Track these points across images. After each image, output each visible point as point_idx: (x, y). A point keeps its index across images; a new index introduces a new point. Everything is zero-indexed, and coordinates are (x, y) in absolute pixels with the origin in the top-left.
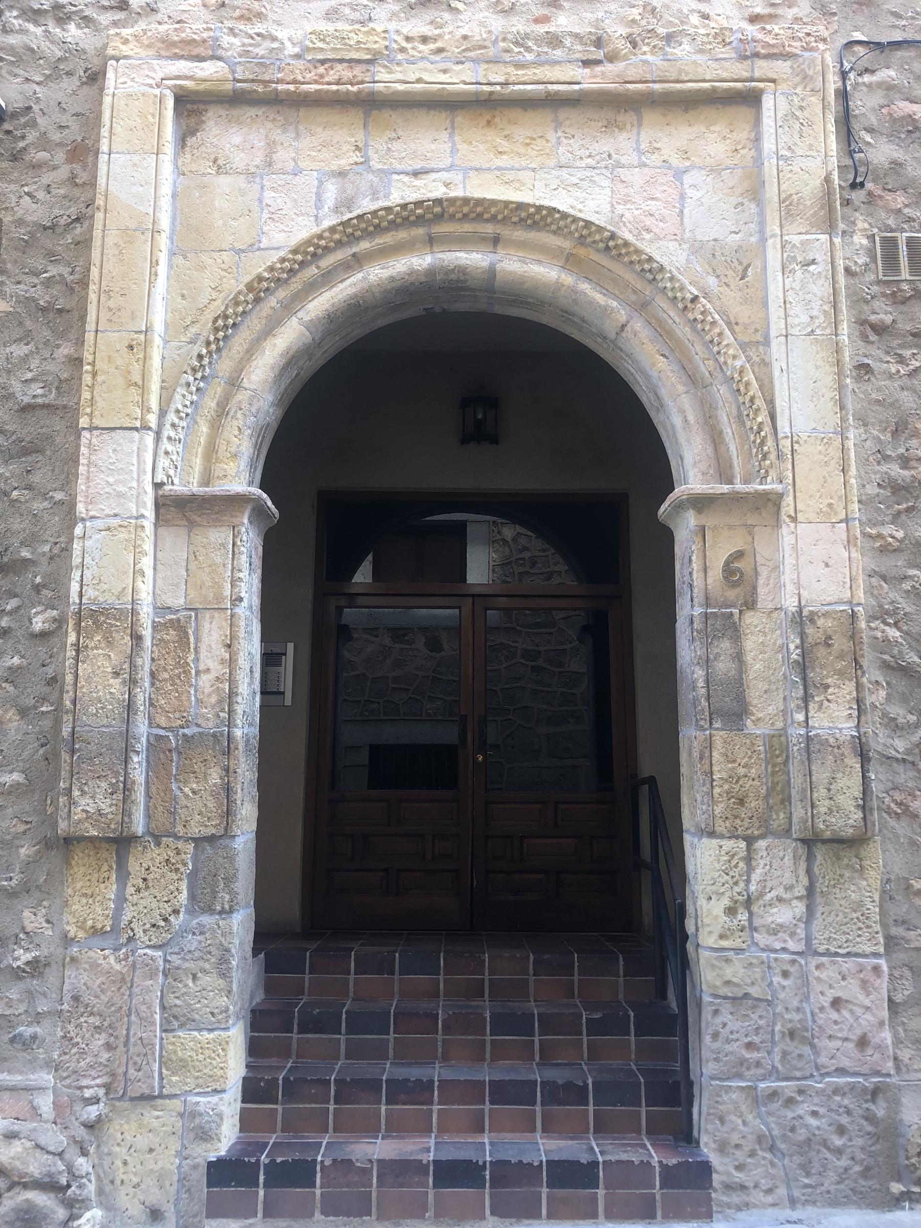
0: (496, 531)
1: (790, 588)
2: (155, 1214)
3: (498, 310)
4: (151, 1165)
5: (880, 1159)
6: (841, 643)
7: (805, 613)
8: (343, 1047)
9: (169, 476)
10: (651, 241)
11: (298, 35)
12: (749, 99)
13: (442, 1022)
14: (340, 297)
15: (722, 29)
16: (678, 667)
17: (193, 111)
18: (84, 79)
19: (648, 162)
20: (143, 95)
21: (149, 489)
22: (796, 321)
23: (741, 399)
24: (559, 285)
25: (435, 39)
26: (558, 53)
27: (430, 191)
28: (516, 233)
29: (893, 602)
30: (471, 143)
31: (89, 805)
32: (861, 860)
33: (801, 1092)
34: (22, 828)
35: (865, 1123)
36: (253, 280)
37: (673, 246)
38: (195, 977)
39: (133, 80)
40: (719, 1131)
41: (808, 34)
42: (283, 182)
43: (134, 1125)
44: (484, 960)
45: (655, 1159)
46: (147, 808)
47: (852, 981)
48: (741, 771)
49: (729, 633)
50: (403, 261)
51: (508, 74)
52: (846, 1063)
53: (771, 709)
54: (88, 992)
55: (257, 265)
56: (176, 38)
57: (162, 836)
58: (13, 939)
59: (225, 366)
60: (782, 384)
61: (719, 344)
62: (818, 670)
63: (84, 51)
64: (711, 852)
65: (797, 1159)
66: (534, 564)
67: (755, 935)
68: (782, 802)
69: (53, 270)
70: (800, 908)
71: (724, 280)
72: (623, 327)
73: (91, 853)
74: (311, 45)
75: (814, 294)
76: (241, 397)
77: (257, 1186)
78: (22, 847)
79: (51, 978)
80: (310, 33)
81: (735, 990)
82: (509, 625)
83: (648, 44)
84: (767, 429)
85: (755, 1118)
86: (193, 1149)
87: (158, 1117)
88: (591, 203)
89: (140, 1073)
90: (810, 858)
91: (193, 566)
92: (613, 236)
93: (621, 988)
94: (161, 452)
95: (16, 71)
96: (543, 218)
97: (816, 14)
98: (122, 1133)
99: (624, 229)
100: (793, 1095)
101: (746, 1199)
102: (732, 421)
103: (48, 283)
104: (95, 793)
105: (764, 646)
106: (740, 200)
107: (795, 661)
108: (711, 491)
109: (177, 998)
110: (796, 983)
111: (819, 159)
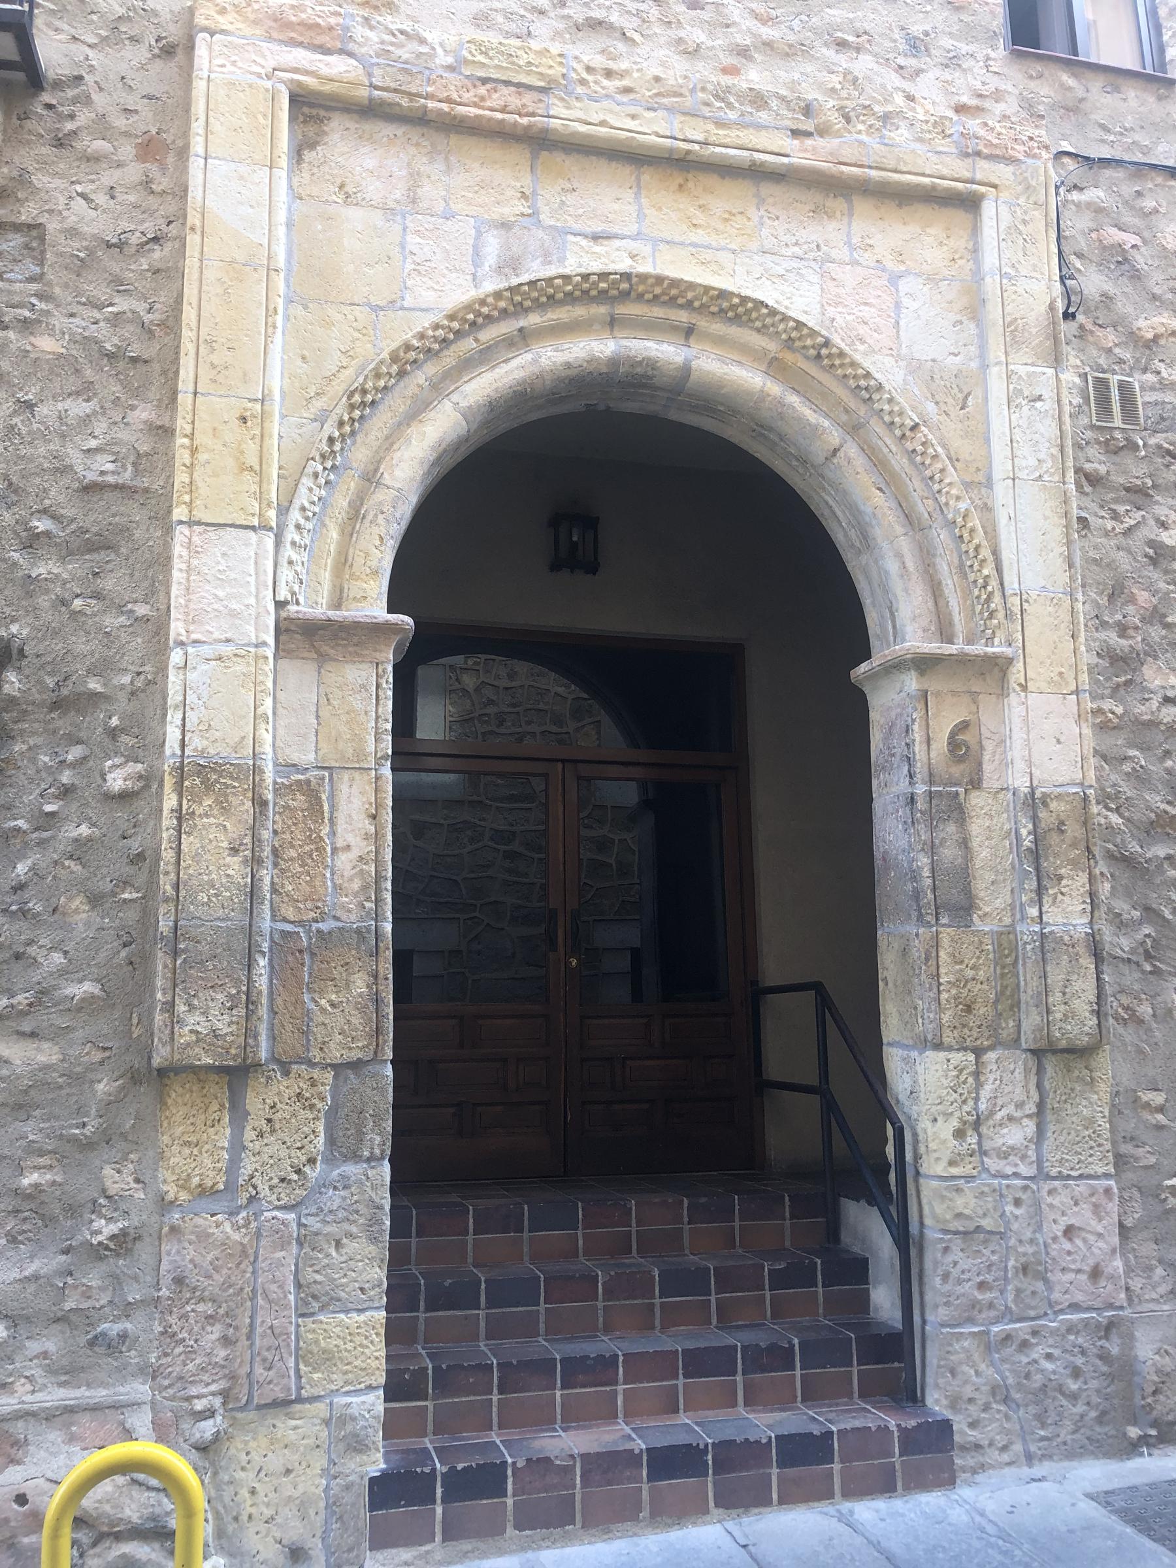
0: (454, 678)
1: (1020, 765)
2: (296, 1553)
3: (674, 415)
4: (289, 1491)
5: (1116, 1401)
6: (1073, 830)
7: (1038, 795)
8: (482, 1324)
9: (293, 594)
10: (865, 354)
11: (452, 41)
12: (967, 203)
13: (604, 1284)
14: (506, 380)
15: (942, 117)
16: (877, 854)
17: (311, 117)
18: (156, 51)
19: (861, 260)
20: (251, 86)
21: (271, 607)
22: (1024, 463)
23: (964, 547)
24: (763, 395)
25: (622, 75)
26: (763, 116)
27: (613, 262)
28: (714, 326)
29: (1115, 785)
30: (660, 208)
31: (202, 1022)
32: (1091, 1071)
33: (1035, 1333)
34: (98, 1056)
35: (1099, 1363)
36: (398, 349)
37: (889, 361)
38: (338, 1244)
39: (234, 63)
40: (951, 1385)
41: (1031, 139)
42: (432, 227)
43: (264, 1442)
44: (631, 1209)
45: (892, 1424)
46: (271, 1028)
47: (1085, 1206)
48: (970, 973)
49: (955, 814)
50: (582, 345)
51: (707, 132)
52: (1079, 1297)
53: (999, 903)
54: (196, 1271)
55: (405, 329)
56: (293, 19)
57: (291, 1063)
58: (90, 1205)
59: (359, 455)
60: (1010, 533)
61: (941, 481)
62: (1051, 859)
63: (155, 13)
64: (938, 1067)
65: (1032, 1409)
66: (501, 723)
67: (985, 1159)
68: (1011, 1007)
69: (123, 304)
70: (1030, 1127)
71: (944, 407)
72: (836, 451)
73: (194, 1088)
74: (470, 58)
75: (1042, 434)
76: (381, 495)
77: (434, 1502)
78: (99, 1082)
79: (144, 1256)
80: (468, 42)
81: (967, 1223)
82: (475, 798)
83: (863, 122)
84: (993, 584)
85: (988, 1366)
86: (344, 1464)
87: (295, 1428)
88: (799, 299)
89: (271, 1373)
90: (1040, 1071)
91: (325, 712)
92: (827, 343)
93: (788, 1233)
94: (283, 562)
95: (58, 23)
96: (748, 312)
97: (1024, 114)
98: (248, 1454)
99: (836, 335)
100: (1027, 1337)
101: (981, 1459)
102: (954, 571)
103: (116, 320)
104: (208, 1008)
105: (991, 833)
106: (959, 318)
107: (1029, 849)
108: (939, 651)
109: (317, 1272)
110: (1028, 1212)
111: (1043, 282)
